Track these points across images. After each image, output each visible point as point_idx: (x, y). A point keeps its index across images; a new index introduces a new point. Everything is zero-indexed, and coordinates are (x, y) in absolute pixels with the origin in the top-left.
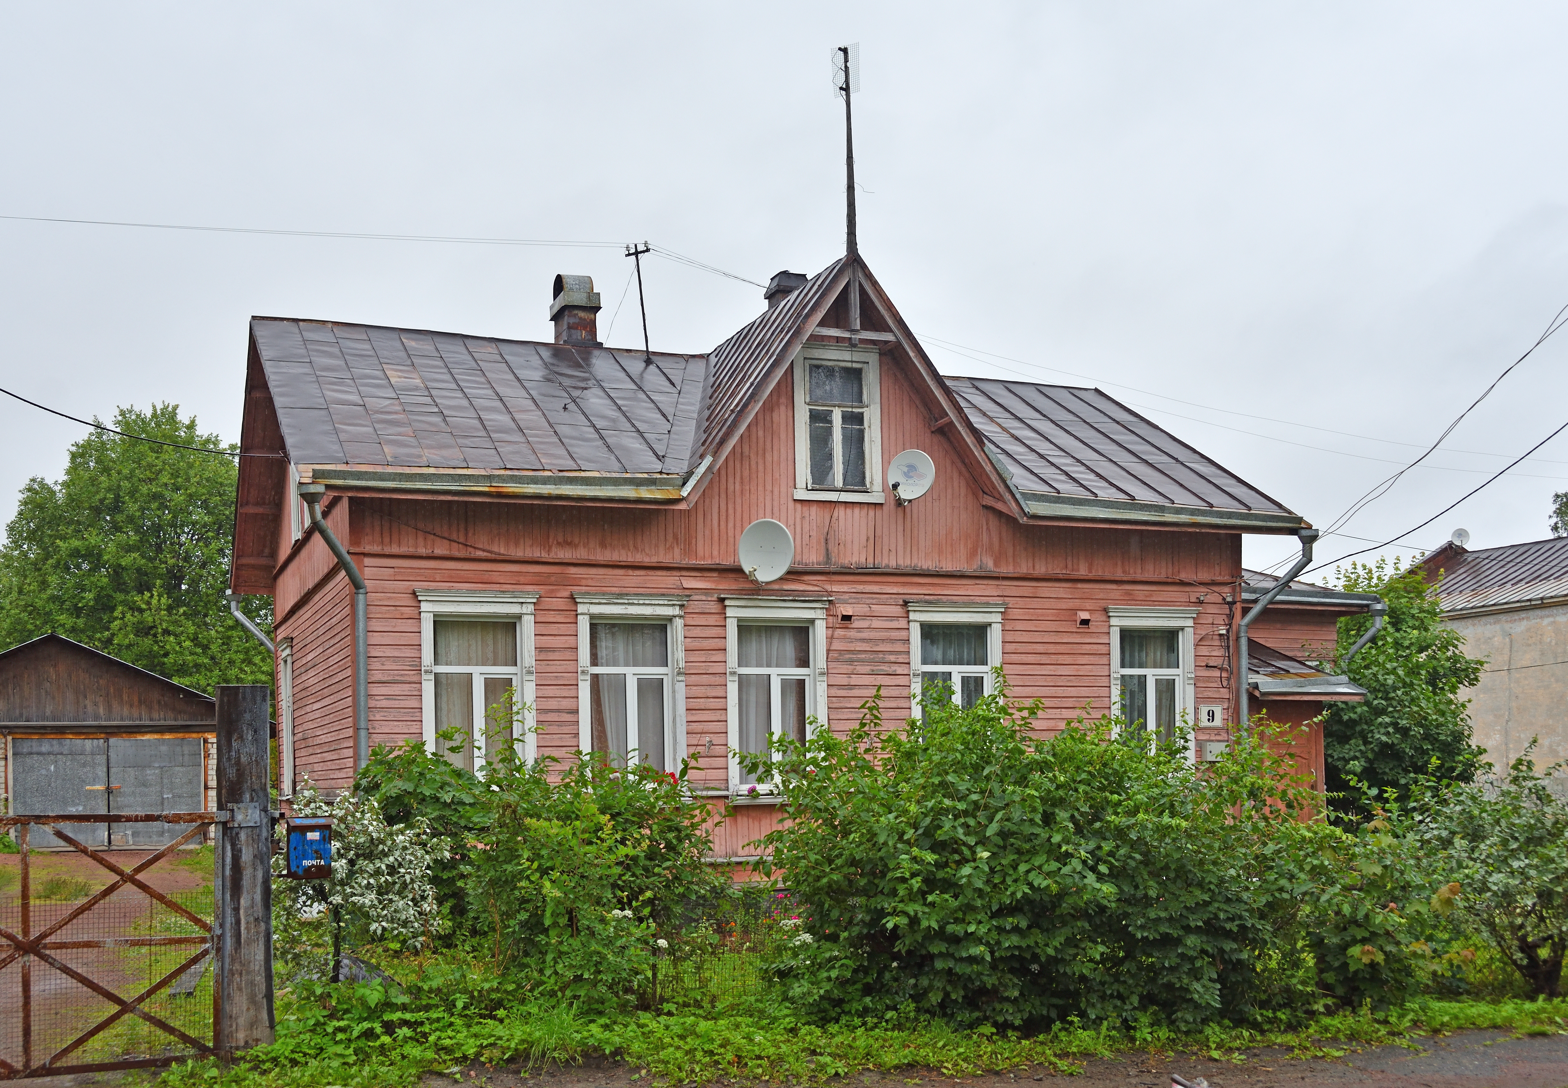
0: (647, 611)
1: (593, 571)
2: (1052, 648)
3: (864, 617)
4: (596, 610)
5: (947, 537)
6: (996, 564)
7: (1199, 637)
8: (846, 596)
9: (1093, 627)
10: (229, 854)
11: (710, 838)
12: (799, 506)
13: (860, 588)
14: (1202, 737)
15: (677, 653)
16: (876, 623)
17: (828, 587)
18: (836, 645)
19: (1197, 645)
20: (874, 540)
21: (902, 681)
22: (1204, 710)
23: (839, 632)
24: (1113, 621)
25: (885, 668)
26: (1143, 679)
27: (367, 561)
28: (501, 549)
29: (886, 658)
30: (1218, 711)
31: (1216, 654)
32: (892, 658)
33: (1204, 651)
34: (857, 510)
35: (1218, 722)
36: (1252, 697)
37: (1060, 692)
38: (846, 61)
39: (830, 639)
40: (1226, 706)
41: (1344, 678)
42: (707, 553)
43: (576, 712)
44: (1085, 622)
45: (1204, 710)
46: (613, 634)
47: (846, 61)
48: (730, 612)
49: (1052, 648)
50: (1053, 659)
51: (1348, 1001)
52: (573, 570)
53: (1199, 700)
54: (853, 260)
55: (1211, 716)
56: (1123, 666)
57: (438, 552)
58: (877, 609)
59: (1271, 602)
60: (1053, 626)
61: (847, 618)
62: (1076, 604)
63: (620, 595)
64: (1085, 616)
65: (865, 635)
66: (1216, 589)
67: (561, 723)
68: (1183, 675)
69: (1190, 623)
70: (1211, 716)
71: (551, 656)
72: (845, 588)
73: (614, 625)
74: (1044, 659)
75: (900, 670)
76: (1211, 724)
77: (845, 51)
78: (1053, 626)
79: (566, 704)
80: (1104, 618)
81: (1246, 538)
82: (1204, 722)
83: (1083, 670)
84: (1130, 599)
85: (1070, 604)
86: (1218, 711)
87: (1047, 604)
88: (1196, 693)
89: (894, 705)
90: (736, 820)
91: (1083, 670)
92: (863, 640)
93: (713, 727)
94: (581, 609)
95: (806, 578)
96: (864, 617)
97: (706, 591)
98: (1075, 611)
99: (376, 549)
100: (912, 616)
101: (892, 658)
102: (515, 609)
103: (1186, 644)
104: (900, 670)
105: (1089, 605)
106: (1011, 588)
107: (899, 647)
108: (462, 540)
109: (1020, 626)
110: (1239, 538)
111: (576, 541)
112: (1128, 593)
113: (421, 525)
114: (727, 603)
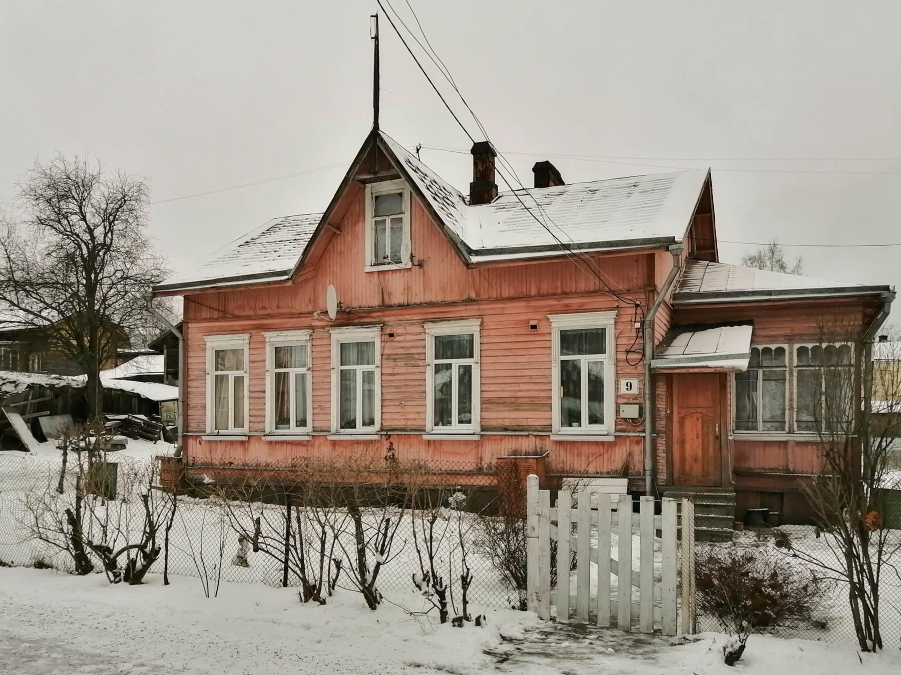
2: (513, 346)
10: (150, 506)
16: (409, 337)
29: (413, 358)
30: (635, 383)
35: (635, 390)
39: (383, 348)
44: (534, 327)
45: (623, 382)
46: (787, 470)
49: (513, 346)
51: (749, 562)
60: (513, 331)
61: (391, 335)
65: (402, 344)
73: (232, 442)
75: (421, 363)
76: (629, 392)
78: (513, 331)
81: (40, 419)
82: (623, 390)
83: (533, 359)
91: (533, 359)
92: (403, 348)
98: (528, 321)
109: (492, 333)
110: (38, 421)
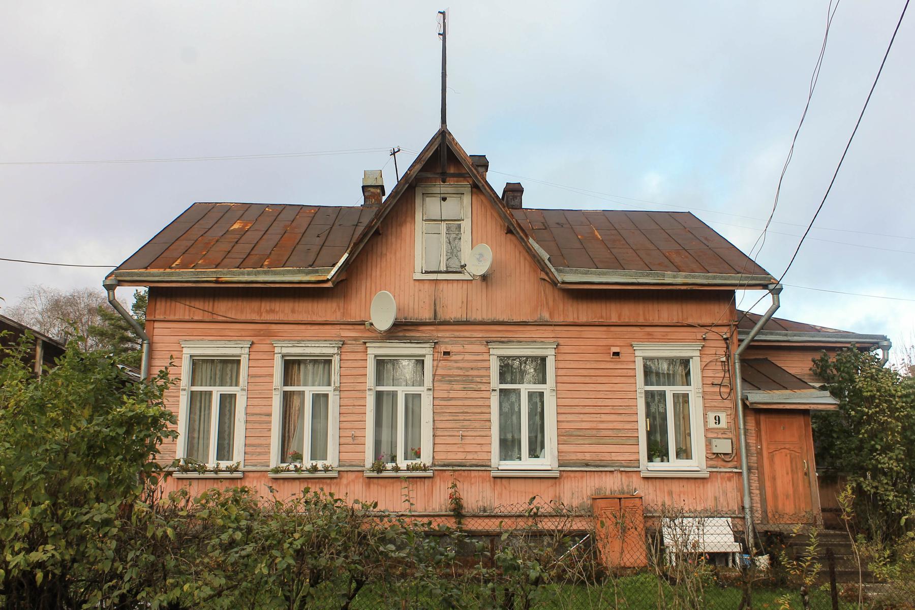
0: (317, 351)
1: (286, 327)
2: (592, 372)
3: (459, 353)
4: (285, 351)
5: (519, 295)
6: (551, 315)
7: (704, 364)
8: (447, 340)
9: (623, 357)
11: (336, 497)
12: (417, 283)
13: (457, 334)
14: (710, 435)
15: (335, 378)
16: (468, 357)
17: (435, 334)
18: (440, 372)
19: (703, 370)
20: (467, 303)
21: (484, 394)
22: (711, 416)
23: (442, 363)
24: (637, 353)
25: (473, 386)
26: (663, 394)
27: (157, 325)
28: (232, 315)
30: (723, 416)
31: (718, 374)
32: (478, 380)
33: (709, 373)
34: (455, 284)
35: (723, 424)
36: (745, 406)
37: (600, 402)
38: (444, 19)
39: (435, 368)
40: (729, 413)
41: (827, 393)
42: (355, 314)
43: (270, 415)
44: (616, 354)
47: (444, 19)
48: (369, 351)
49: (592, 372)
50: (594, 379)
52: (274, 327)
53: (706, 409)
54: (443, 135)
55: (718, 420)
56: (646, 384)
57: (196, 318)
58: (469, 348)
59: (753, 340)
61: (447, 353)
62: (611, 342)
63: (299, 341)
64: (616, 350)
66: (714, 329)
67: (260, 422)
68: (694, 391)
69: (698, 353)
70: (718, 420)
71: (258, 380)
72: (447, 334)
74: (587, 380)
75: (483, 387)
76: (717, 426)
77: (443, 13)
79: (265, 410)
80: (631, 351)
84: (651, 338)
85: (604, 342)
86: (723, 416)
87: (589, 342)
88: (704, 404)
89: (479, 411)
90: (369, 487)
93: (357, 425)
94: (277, 350)
95: (421, 328)
96: (459, 353)
97: (356, 339)
99: (162, 317)
100: (492, 351)
101: (478, 380)
102: (237, 351)
103: (695, 367)
104: (483, 387)
105: (619, 342)
106: (562, 331)
107: (483, 372)
108: (210, 310)
110: (734, 292)
111: (277, 309)
112: (649, 334)
113: (188, 303)
114: (368, 345)
